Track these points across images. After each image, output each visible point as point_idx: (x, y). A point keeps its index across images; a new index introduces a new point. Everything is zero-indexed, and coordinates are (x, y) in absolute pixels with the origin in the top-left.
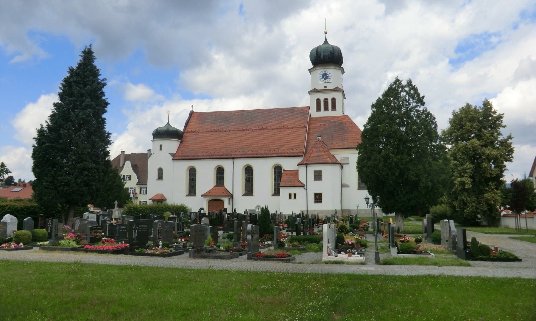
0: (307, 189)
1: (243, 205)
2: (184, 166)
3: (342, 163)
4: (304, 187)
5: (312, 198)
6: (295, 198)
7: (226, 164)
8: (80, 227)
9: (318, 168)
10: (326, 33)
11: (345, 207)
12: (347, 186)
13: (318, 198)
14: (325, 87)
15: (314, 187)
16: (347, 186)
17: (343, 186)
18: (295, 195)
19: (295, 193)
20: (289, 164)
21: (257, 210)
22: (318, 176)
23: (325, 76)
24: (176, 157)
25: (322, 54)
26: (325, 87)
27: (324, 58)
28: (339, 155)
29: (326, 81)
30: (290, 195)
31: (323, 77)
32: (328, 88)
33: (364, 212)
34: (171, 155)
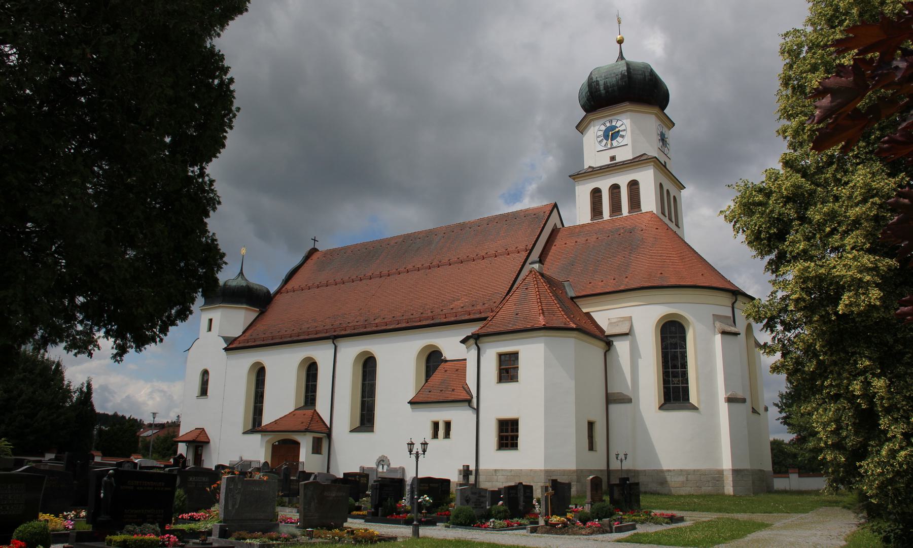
0: (477, 410)
1: (352, 454)
2: (245, 361)
3: (608, 332)
4: (469, 401)
5: (490, 435)
6: (447, 435)
7: (322, 354)
8: (577, 491)
9: (507, 347)
10: (620, 42)
11: (615, 465)
12: (626, 400)
13: (508, 433)
14: (613, 158)
15: (498, 400)
16: (626, 400)
17: (611, 399)
18: (448, 425)
19: (447, 419)
20: (451, 344)
21: (380, 469)
22: (508, 369)
23: (611, 134)
24: (233, 346)
25: (601, 83)
26: (613, 158)
27: (607, 92)
28: (606, 316)
29: (615, 143)
30: (436, 425)
31: (606, 136)
32: (618, 160)
33: (682, 479)
34: (226, 339)
